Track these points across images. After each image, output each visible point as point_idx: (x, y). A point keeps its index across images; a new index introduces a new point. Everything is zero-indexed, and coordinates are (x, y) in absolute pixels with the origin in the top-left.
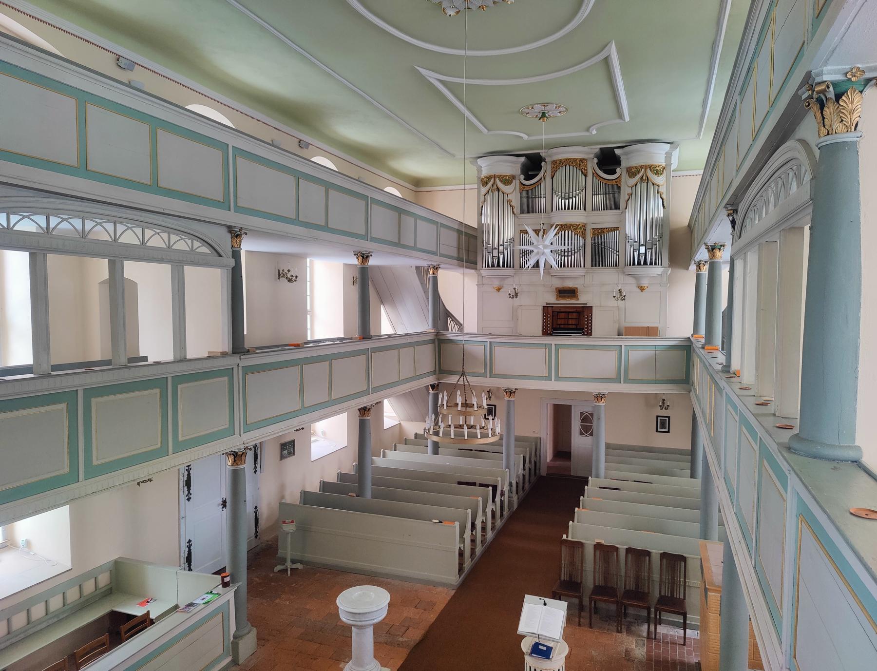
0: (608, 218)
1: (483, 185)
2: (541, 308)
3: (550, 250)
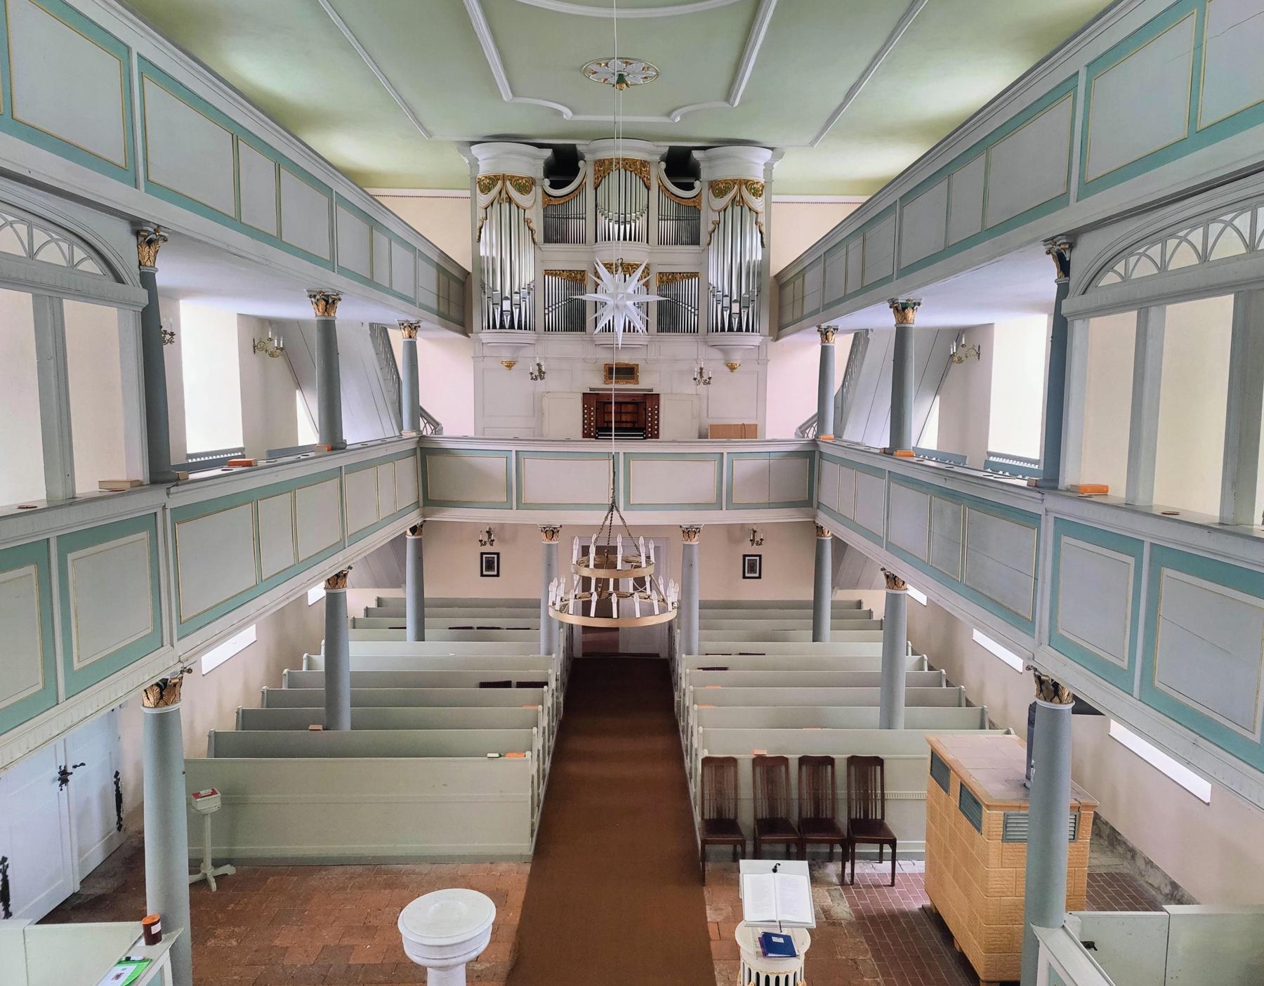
0: (680, 258)
1: (482, 191)
2: (580, 396)
3: (633, 302)
